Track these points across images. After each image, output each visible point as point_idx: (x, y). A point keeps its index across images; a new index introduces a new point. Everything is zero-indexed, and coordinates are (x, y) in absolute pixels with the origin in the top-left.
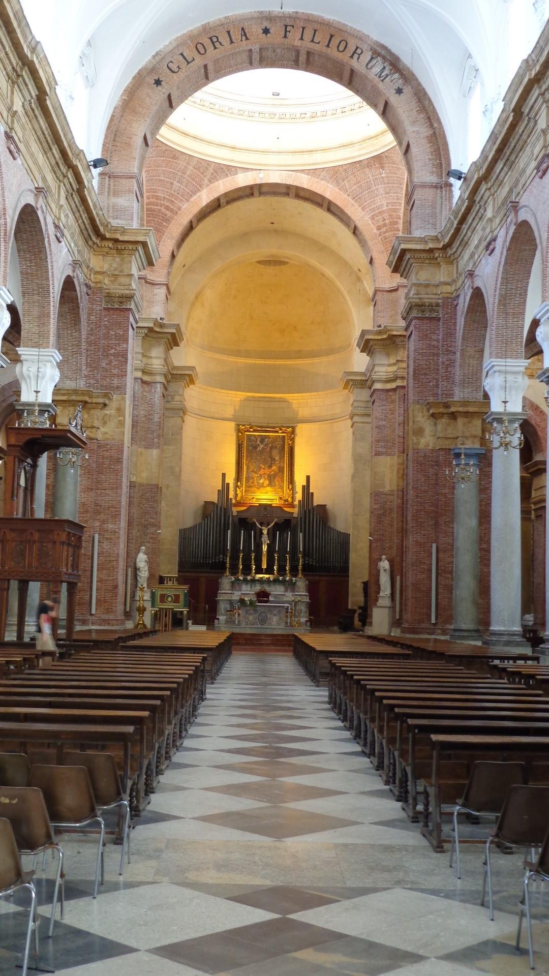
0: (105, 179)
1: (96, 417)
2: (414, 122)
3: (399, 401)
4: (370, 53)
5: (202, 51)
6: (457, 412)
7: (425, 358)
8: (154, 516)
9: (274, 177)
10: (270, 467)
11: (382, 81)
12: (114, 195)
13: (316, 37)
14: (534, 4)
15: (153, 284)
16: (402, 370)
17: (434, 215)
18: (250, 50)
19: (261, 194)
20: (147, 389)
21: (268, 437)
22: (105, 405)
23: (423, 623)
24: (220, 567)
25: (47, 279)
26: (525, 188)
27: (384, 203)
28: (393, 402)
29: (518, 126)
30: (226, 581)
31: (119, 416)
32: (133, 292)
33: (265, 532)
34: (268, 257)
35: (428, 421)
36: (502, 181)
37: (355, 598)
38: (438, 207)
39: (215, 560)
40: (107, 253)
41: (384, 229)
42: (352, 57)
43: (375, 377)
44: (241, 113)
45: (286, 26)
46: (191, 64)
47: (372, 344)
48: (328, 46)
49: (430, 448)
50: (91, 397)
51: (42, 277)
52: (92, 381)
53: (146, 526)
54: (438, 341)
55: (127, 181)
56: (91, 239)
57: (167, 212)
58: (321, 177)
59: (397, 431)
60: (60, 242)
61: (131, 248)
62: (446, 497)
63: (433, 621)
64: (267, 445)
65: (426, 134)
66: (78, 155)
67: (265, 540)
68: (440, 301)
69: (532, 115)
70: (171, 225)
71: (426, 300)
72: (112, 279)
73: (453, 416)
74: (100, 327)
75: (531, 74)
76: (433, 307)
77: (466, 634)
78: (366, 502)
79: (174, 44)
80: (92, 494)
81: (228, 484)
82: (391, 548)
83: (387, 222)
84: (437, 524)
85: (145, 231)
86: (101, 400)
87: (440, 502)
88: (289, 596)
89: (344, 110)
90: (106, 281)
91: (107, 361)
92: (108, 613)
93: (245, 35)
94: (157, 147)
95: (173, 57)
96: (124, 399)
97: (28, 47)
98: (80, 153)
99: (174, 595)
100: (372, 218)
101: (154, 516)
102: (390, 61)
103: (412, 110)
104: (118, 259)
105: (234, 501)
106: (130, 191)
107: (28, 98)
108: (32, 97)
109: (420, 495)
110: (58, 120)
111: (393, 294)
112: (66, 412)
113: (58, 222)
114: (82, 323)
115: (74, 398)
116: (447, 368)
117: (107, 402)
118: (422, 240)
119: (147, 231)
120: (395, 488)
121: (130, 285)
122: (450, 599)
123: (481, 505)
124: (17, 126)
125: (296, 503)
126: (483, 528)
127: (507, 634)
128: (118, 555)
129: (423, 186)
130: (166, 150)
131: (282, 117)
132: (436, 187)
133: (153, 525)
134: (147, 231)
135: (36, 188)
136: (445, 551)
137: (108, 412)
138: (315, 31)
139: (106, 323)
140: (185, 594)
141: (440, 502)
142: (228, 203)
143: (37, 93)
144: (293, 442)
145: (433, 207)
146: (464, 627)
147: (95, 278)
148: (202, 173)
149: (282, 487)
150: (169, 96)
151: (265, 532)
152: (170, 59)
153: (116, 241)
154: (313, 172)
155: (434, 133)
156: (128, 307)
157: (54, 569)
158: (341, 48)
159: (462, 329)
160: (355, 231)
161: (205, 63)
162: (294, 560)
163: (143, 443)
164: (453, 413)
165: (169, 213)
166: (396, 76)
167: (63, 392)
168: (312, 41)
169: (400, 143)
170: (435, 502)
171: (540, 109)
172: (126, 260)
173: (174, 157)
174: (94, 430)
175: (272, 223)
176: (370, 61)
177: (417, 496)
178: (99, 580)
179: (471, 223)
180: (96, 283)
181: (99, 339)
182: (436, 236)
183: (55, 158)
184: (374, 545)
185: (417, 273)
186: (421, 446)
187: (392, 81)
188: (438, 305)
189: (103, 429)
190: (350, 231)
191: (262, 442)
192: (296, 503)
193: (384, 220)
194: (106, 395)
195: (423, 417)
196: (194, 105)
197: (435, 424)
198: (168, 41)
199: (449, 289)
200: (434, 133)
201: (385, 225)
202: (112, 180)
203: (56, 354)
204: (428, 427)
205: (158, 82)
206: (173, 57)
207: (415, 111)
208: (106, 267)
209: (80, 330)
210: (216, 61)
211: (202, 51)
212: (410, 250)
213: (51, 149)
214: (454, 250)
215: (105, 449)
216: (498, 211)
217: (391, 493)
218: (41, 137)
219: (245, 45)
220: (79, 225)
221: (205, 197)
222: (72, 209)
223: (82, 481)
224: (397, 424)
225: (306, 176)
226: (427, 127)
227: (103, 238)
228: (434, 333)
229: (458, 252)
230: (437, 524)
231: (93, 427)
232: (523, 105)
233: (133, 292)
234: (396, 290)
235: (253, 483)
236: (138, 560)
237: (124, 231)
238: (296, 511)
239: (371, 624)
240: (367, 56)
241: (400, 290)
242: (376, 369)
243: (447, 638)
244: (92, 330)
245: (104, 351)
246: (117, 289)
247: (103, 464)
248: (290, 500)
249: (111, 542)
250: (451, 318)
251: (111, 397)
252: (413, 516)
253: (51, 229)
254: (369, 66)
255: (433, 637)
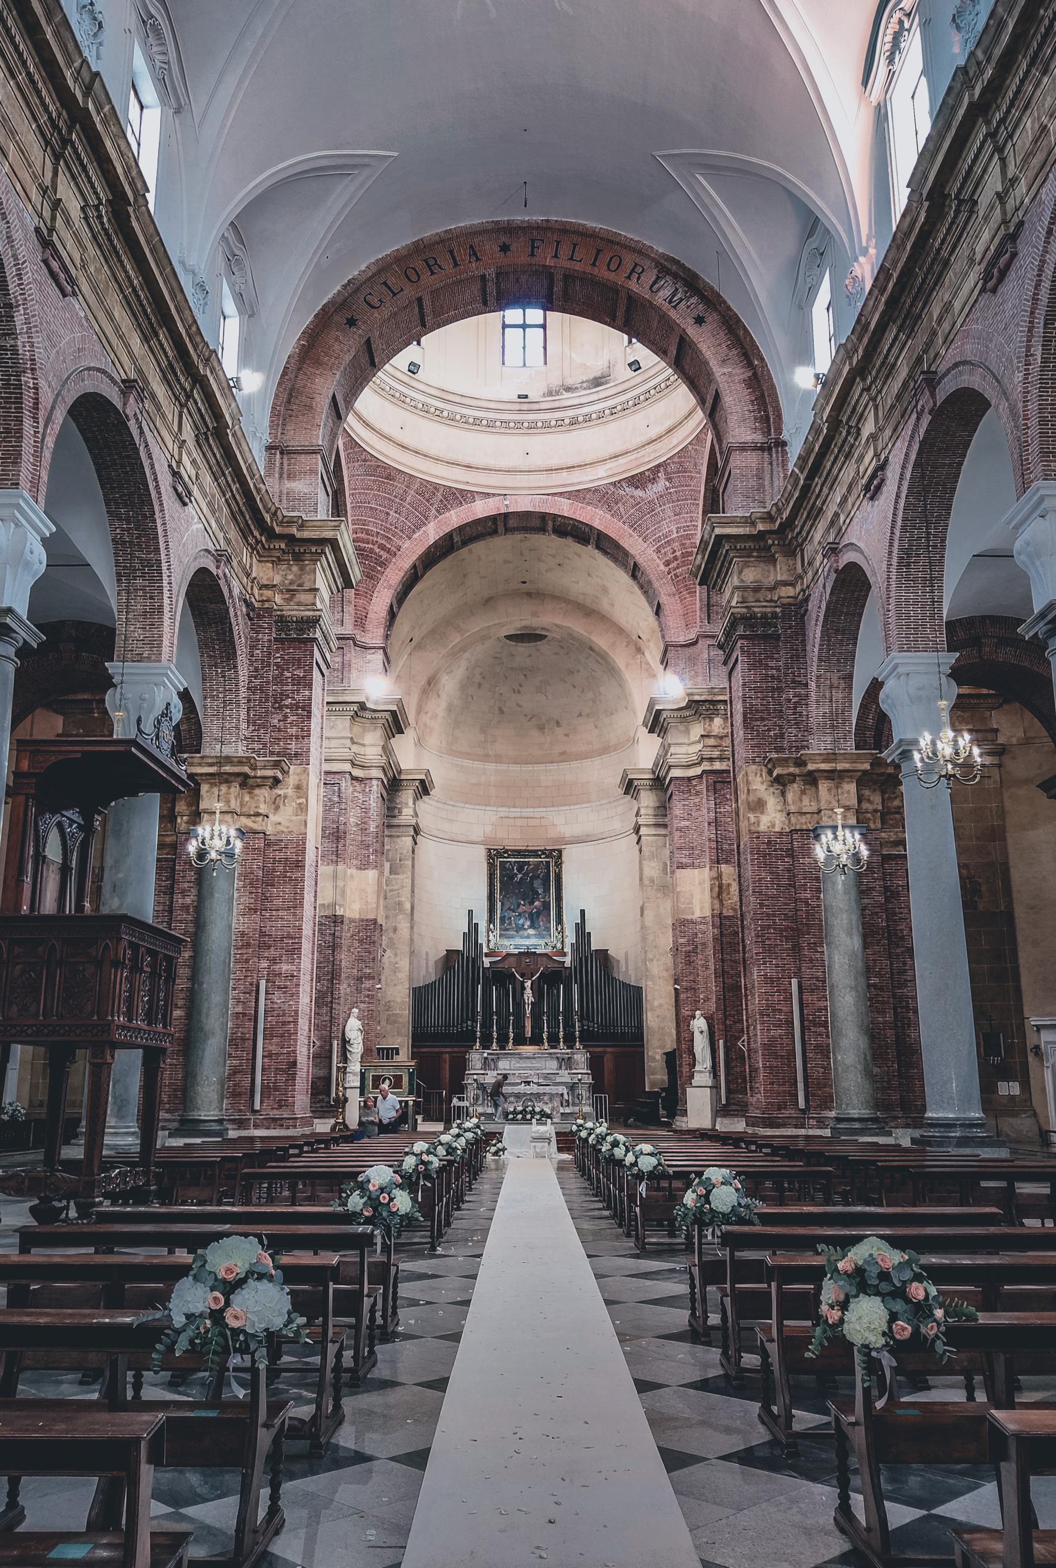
0: (275, 454)
1: (262, 799)
2: (724, 361)
3: (707, 791)
4: (655, 271)
5: (414, 278)
6: (818, 771)
7: (759, 695)
8: (371, 965)
9: (523, 505)
10: (532, 903)
11: (675, 307)
12: (289, 477)
13: (576, 254)
14: (954, 20)
15: (365, 648)
16: (709, 749)
17: (760, 488)
18: (483, 277)
19: (508, 530)
20: (358, 787)
21: (528, 863)
22: (276, 782)
23: (785, 1108)
24: (467, 1039)
25: (157, 550)
26: (948, 342)
27: (674, 528)
28: (697, 793)
29: (934, 233)
30: (476, 1058)
31: (299, 798)
32: (317, 613)
33: (528, 984)
34: (520, 629)
35: (772, 789)
36: (895, 364)
37: (655, 1075)
38: (767, 477)
39: (462, 1028)
40: (278, 557)
41: (673, 565)
42: (629, 277)
43: (671, 761)
44: (477, 422)
45: (533, 241)
46: (398, 296)
47: (727, 547)
48: (594, 264)
49: (777, 829)
50: (254, 768)
51: (148, 547)
52: (256, 746)
53: (359, 979)
54: (778, 669)
55: (309, 457)
56: (252, 533)
57: (382, 553)
58: (587, 500)
59: (706, 833)
60: (185, 504)
61: (313, 550)
62: (807, 904)
63: (802, 1104)
64: (526, 874)
65: (742, 377)
66: (208, 360)
67: (529, 996)
68: (778, 610)
69: (965, 195)
70: (388, 570)
71: (757, 610)
72: (287, 596)
73: (812, 779)
74: (269, 665)
75: (973, 95)
76: (766, 620)
77: (857, 1125)
78: (666, 941)
79: (374, 269)
80: (256, 917)
81: (476, 925)
82: (707, 999)
83: (678, 554)
84: (796, 949)
85: (334, 524)
86: (269, 773)
87: (799, 913)
88: (565, 1076)
89: (614, 411)
90: (278, 599)
91: (280, 717)
92: (280, 1107)
93: (475, 254)
94: (365, 461)
95: (372, 288)
96: (306, 771)
97: (76, 80)
98: (210, 357)
99: (394, 1076)
100: (658, 551)
101: (371, 965)
102: (683, 279)
103: (719, 345)
104: (295, 569)
105: (485, 950)
106: (313, 472)
107: (92, 201)
108: (208, 429)
109: (766, 903)
110: (161, 274)
111: (691, 650)
112: (215, 790)
113: (178, 467)
114: (239, 658)
115: (228, 769)
116: (795, 708)
117: (280, 775)
118: (750, 521)
119: (336, 524)
120: (708, 913)
121: (314, 604)
122: (827, 1068)
123: (863, 916)
124: (185, 459)
125: (568, 949)
126: (869, 951)
127: (961, 1125)
128: (296, 1012)
129: (743, 448)
130: (378, 466)
131: (533, 426)
132: (762, 449)
133: (370, 977)
134: (336, 524)
135: (123, 381)
136: (813, 991)
137: (281, 792)
138: (575, 245)
139: (279, 660)
140: (411, 1075)
141: (799, 913)
142: (465, 543)
143: (111, 198)
144: (560, 871)
145: (760, 477)
146: (854, 1113)
147: (261, 595)
148: (428, 501)
149: (548, 929)
150: (368, 342)
151: (528, 984)
152: (369, 290)
153: (291, 539)
154: (576, 495)
155: (755, 374)
156: (311, 635)
157: (95, 1018)
158: (613, 267)
159: (817, 646)
160: (635, 572)
161: (418, 296)
162: (569, 1025)
163: (355, 862)
164: (810, 773)
165: (384, 555)
166: (694, 300)
167: (210, 761)
168: (571, 259)
169: (702, 401)
170: (790, 914)
171: (985, 171)
172: (307, 568)
173: (389, 477)
174: (260, 819)
175: (524, 582)
176: (655, 283)
177: (761, 905)
178: (266, 1054)
179: (830, 470)
180: (263, 601)
181: (268, 683)
182: (769, 513)
183: (167, 356)
184: (682, 996)
185: (740, 572)
186: (762, 828)
187: (688, 307)
188: (775, 615)
189: (273, 818)
190: (628, 573)
191: (520, 870)
192: (568, 949)
193: (674, 551)
194: (277, 765)
195: (762, 783)
196: (414, 410)
197: (783, 794)
198: (365, 265)
199: (790, 591)
200: (755, 374)
201: (676, 558)
202: (285, 457)
203: (172, 672)
204: (772, 803)
205: (352, 322)
206: (372, 288)
207: (724, 346)
208: (277, 580)
209: (235, 667)
210: (435, 293)
211: (414, 278)
212: (728, 537)
213: (157, 335)
214: (797, 530)
215: (277, 847)
216: (887, 418)
217: (703, 921)
218: (132, 299)
219: (474, 269)
220: (226, 500)
221: (432, 533)
222: (211, 468)
223: (240, 897)
224: (706, 824)
225: (566, 500)
226: (743, 367)
227: (271, 535)
228: (772, 658)
229: (804, 534)
230: (796, 949)
231: (258, 815)
232: (947, 182)
233: (317, 613)
234: (694, 643)
235: (510, 924)
236: (347, 1028)
237: (302, 525)
238: (568, 961)
239: (684, 1113)
240: (650, 277)
241: (700, 642)
242: (672, 750)
243: (827, 1133)
244: (256, 670)
245: (276, 702)
246: (293, 612)
247: (274, 870)
248: (559, 946)
249: (284, 993)
250: (797, 634)
251: (286, 768)
252: (757, 936)
253: (165, 479)
254: (654, 288)
255: (802, 1132)
